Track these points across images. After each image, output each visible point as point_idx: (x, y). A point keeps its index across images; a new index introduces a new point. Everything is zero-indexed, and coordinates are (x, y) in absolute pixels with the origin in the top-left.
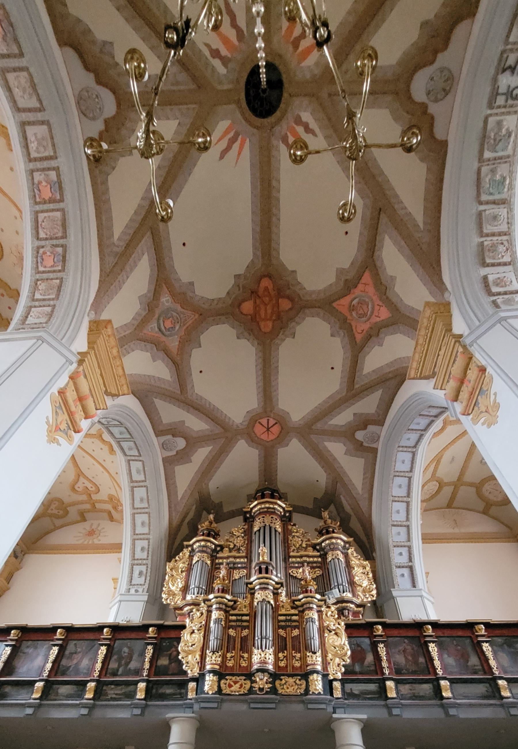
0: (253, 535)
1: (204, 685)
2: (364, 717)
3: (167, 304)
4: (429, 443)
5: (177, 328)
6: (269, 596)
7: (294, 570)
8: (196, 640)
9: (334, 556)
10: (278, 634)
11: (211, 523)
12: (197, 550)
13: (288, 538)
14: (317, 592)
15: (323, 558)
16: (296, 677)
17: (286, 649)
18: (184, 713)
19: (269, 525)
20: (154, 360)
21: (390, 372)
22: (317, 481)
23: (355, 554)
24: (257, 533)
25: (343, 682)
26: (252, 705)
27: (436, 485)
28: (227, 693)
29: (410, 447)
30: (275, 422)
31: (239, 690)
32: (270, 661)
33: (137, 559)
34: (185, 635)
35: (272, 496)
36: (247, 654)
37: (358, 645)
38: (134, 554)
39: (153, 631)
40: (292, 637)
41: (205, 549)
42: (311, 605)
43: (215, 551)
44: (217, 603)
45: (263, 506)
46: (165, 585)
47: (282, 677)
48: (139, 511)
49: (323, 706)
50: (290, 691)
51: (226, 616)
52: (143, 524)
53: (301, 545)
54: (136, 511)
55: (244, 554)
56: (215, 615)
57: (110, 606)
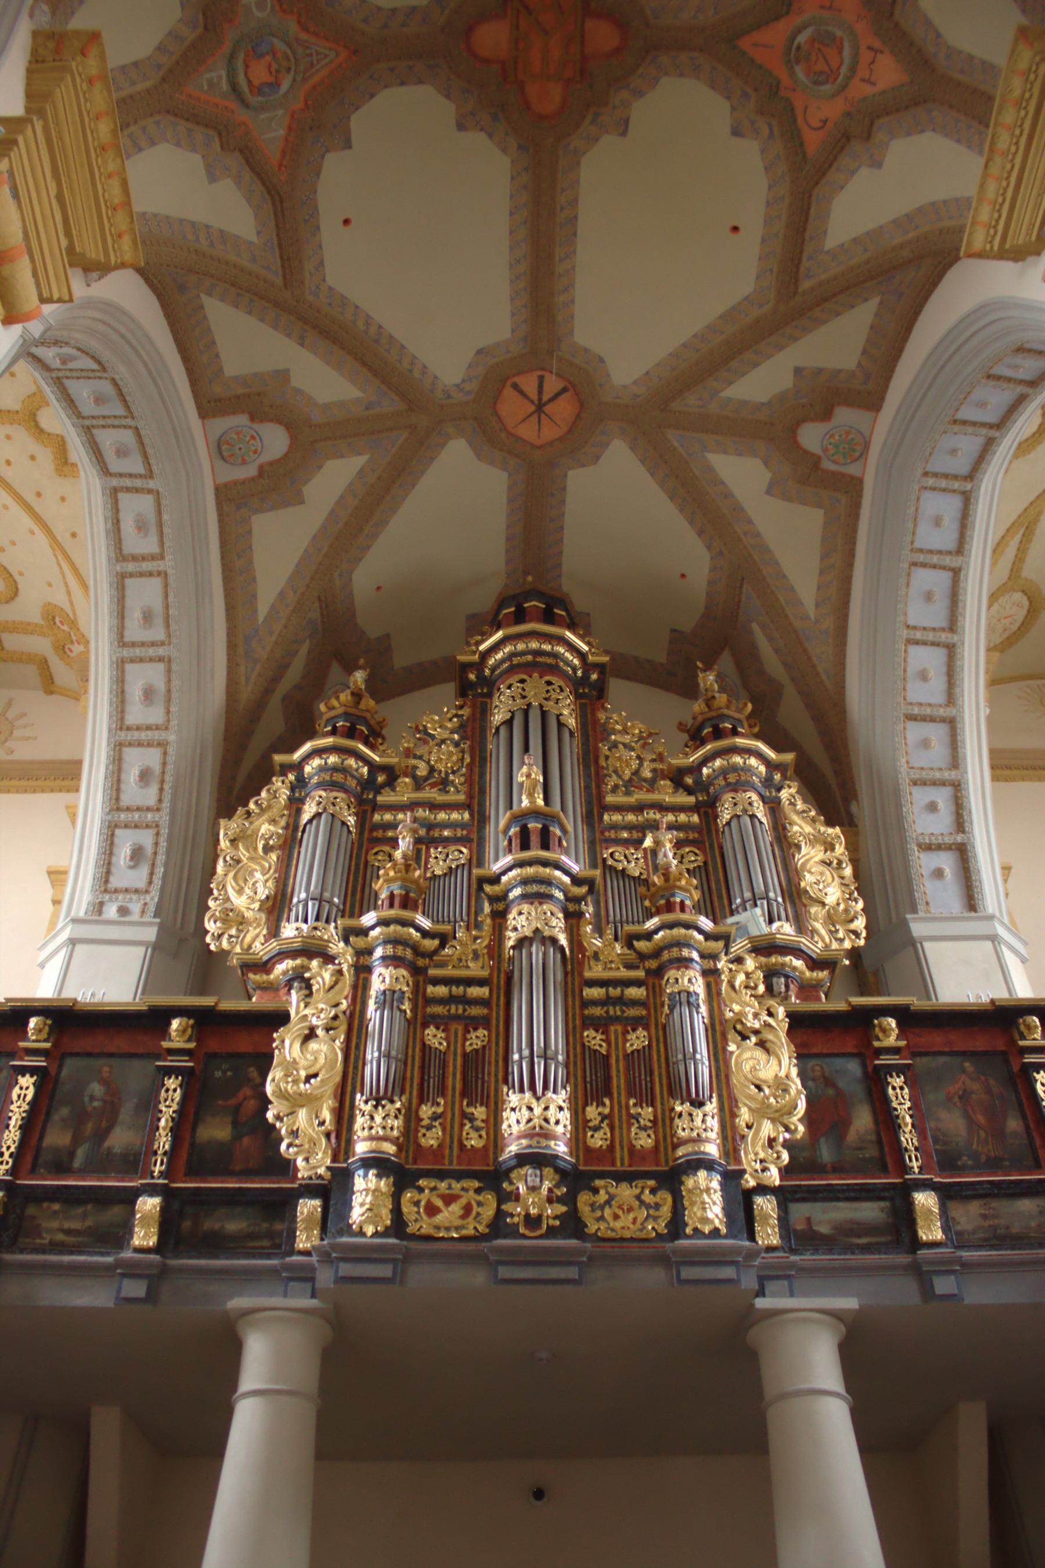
0: (490, 738)
1: (351, 1208)
2: (850, 1303)
3: (259, 14)
4: (1006, 472)
5: (285, 86)
6: (554, 922)
7: (619, 851)
8: (322, 1061)
9: (740, 808)
10: (583, 1045)
11: (357, 696)
12: (315, 780)
13: (597, 750)
14: (700, 908)
15: (706, 813)
16: (640, 1183)
17: (608, 1093)
18: (285, 1295)
19: (541, 706)
20: (212, 178)
21: (902, 246)
22: (683, 576)
23: (800, 805)
24: (503, 731)
25: (784, 1195)
26: (504, 1272)
27: (1019, 605)
28: (423, 1231)
29: (956, 477)
30: (560, 385)
31: (459, 1222)
32: (560, 1129)
33: (128, 809)
34: (287, 1043)
35: (548, 617)
36: (483, 1109)
37: (829, 1082)
38: (118, 790)
39: (184, 1031)
40: (626, 1056)
41: (338, 777)
42: (685, 952)
43: (369, 784)
44: (386, 942)
45: (521, 646)
46: (215, 892)
47: (598, 1183)
48: (138, 652)
49: (729, 1272)
50: (625, 1225)
51: (416, 985)
52: (148, 694)
53: (636, 773)
54: (126, 653)
55: (461, 797)
56: (381, 979)
57: (40, 960)
